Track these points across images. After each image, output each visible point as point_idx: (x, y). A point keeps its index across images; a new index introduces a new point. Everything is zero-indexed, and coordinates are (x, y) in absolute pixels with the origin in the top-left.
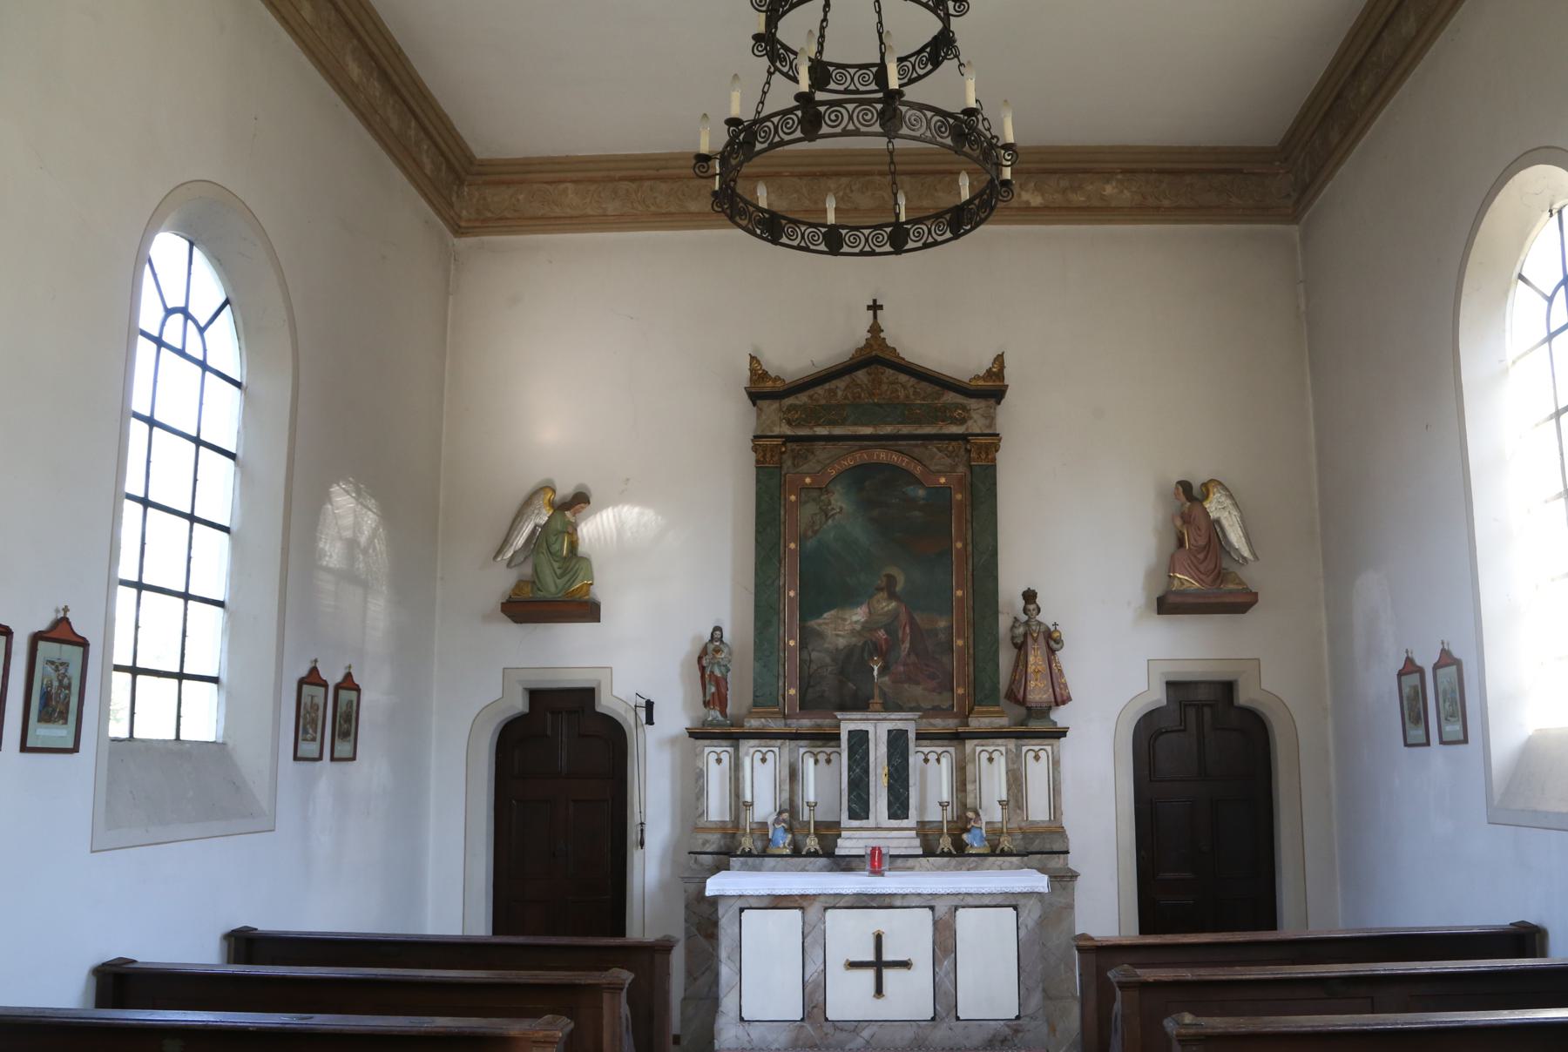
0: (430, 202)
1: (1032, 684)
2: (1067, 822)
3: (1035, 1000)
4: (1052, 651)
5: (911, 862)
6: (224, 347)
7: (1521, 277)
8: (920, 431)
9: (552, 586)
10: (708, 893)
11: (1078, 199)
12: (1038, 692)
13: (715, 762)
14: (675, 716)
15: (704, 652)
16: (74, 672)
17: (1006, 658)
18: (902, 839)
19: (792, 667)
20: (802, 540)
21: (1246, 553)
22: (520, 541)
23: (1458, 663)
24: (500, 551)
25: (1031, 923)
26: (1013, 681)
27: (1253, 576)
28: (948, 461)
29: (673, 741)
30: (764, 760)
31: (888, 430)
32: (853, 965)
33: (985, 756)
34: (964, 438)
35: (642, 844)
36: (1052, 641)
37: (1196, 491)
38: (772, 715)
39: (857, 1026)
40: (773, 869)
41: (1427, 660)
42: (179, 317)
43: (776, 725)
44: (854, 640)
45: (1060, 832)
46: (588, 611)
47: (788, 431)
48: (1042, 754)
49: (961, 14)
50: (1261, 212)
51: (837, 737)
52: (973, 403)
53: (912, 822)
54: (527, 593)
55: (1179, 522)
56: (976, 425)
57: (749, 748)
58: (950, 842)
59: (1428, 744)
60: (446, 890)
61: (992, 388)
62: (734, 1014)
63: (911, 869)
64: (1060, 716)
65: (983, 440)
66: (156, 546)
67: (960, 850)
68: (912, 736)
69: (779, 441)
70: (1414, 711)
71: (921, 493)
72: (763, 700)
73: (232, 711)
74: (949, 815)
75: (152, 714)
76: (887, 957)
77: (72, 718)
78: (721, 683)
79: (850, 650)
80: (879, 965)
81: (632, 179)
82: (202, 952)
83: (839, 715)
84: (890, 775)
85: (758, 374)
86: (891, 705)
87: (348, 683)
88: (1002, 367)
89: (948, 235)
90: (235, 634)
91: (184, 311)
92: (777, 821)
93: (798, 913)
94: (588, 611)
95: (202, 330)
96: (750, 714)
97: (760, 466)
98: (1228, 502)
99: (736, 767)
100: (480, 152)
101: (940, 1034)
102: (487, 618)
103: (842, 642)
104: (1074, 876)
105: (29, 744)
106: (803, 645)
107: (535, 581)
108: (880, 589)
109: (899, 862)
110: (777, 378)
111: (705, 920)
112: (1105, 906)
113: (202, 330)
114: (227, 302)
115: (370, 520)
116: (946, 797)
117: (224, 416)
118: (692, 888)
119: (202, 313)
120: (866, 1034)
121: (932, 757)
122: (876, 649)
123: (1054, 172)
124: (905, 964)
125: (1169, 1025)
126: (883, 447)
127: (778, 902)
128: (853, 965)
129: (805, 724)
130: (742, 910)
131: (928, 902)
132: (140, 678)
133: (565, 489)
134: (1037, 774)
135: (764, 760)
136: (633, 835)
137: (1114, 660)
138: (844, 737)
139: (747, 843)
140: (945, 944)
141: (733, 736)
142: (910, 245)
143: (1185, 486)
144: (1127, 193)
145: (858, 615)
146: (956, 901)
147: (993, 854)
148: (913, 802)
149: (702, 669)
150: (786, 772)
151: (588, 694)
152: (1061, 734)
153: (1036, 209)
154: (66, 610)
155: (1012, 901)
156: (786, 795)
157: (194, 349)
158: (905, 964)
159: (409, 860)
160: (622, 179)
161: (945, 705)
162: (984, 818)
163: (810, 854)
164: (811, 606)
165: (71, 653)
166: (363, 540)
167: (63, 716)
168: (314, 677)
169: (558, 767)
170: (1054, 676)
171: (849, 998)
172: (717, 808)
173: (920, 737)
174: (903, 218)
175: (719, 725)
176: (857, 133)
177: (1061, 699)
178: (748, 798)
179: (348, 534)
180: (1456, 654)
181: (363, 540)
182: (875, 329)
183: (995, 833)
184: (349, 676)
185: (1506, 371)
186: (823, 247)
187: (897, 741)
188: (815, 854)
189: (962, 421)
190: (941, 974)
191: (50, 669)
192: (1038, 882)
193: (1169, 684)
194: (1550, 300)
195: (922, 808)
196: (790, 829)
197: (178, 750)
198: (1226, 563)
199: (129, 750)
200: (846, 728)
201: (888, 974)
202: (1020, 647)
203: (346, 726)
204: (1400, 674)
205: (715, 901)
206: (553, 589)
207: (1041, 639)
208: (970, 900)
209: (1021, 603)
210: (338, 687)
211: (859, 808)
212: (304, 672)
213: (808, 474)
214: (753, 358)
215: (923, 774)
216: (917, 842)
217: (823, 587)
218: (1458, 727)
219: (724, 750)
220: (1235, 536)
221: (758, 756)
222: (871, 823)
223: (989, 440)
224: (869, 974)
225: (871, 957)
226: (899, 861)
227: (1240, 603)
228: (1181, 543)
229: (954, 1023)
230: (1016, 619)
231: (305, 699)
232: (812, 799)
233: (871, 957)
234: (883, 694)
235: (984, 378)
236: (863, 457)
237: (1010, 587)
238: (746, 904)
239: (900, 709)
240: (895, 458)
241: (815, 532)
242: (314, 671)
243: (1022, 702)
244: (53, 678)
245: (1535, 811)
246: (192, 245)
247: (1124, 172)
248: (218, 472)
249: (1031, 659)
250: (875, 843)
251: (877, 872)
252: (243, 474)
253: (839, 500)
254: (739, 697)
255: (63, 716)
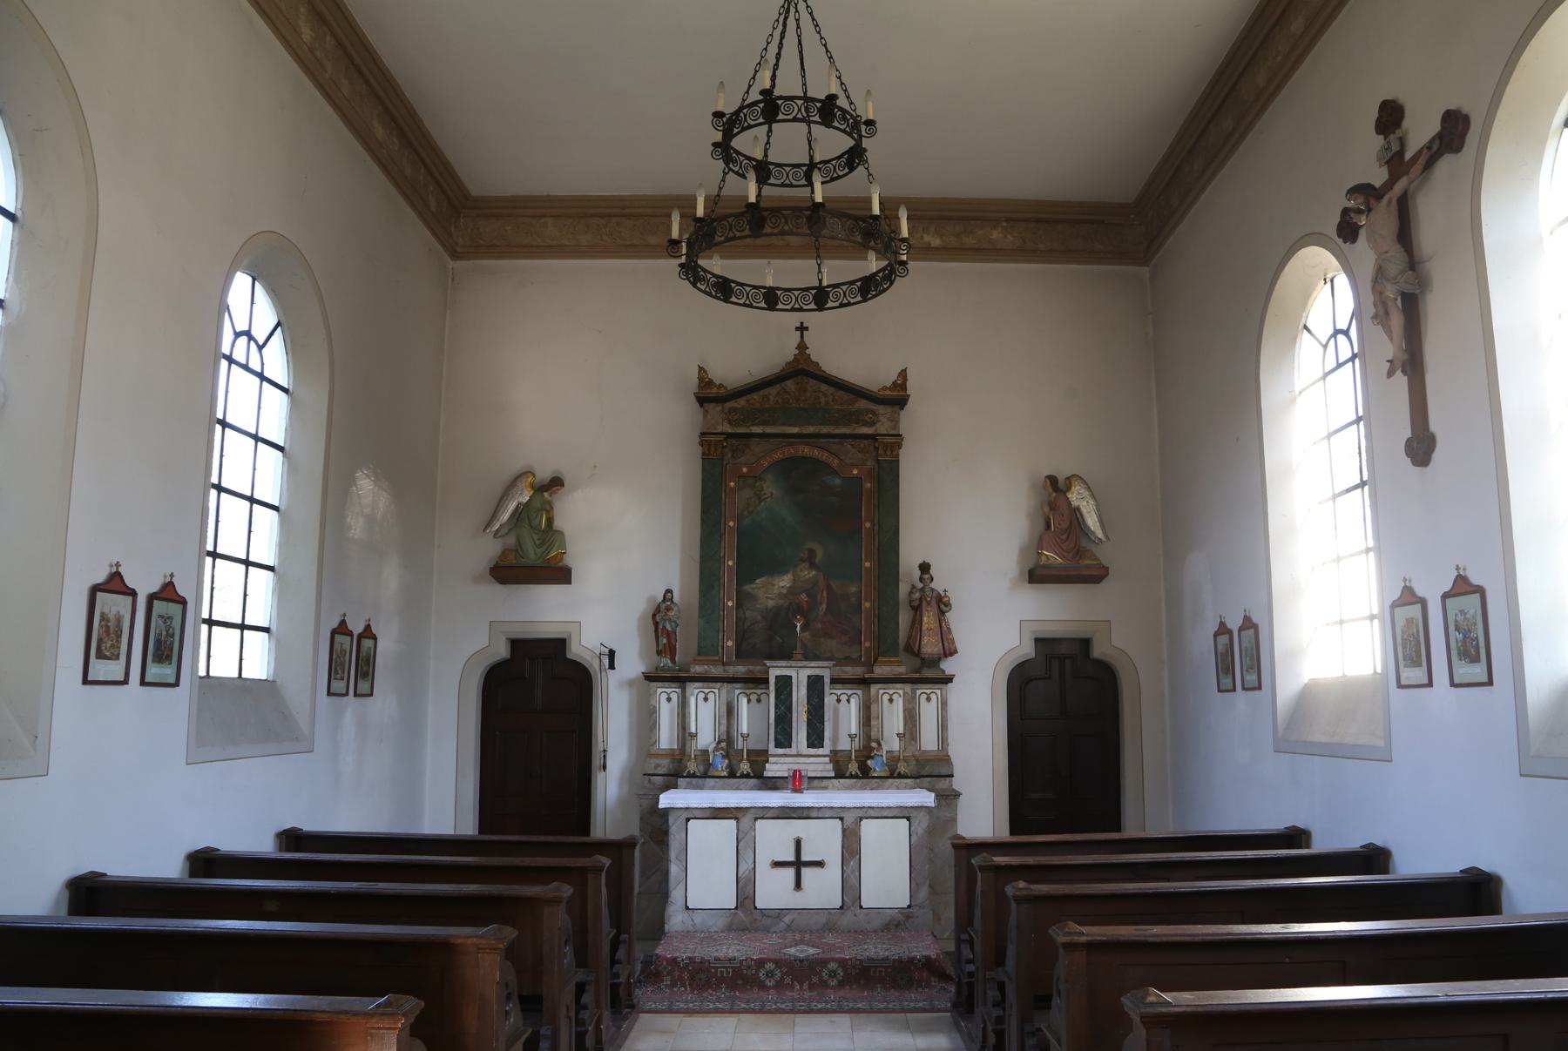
0: (435, 234)
1: (925, 639)
2: (952, 751)
3: (923, 893)
4: (943, 613)
5: (825, 783)
6: (276, 361)
7: (1305, 327)
8: (837, 431)
9: (532, 554)
10: (661, 806)
11: (970, 241)
12: (930, 645)
13: (665, 701)
14: (632, 664)
15: (658, 610)
16: (177, 624)
17: (904, 618)
18: (818, 764)
19: (729, 624)
20: (739, 519)
21: (1100, 534)
22: (505, 516)
23: (1255, 627)
24: (488, 525)
25: (920, 831)
26: (910, 637)
27: (1105, 554)
28: (860, 456)
29: (631, 683)
30: (706, 699)
31: (811, 430)
32: (777, 864)
33: (886, 697)
34: (873, 437)
35: (605, 768)
36: (942, 604)
37: (1061, 484)
38: (714, 663)
39: (780, 913)
40: (713, 788)
41: (1234, 624)
42: (244, 339)
43: (716, 671)
44: (781, 602)
45: (946, 760)
46: (561, 575)
47: (730, 430)
48: (933, 696)
49: (871, 135)
50: (1119, 255)
51: (766, 681)
52: (881, 409)
53: (826, 750)
54: (512, 560)
55: (1046, 509)
56: (882, 428)
57: (695, 692)
58: (858, 766)
59: (1234, 690)
60: (444, 804)
61: (896, 397)
62: (681, 903)
63: (825, 788)
64: (948, 666)
65: (888, 440)
66: (231, 526)
67: (865, 773)
68: (827, 680)
69: (721, 438)
70: (1225, 665)
71: (838, 481)
72: (706, 650)
73: (280, 654)
74: (856, 744)
75: (223, 656)
76: (805, 858)
77: (175, 659)
78: (671, 636)
79: (777, 611)
80: (798, 864)
81: (602, 216)
82: (262, 844)
83: (768, 663)
84: (809, 712)
85: (705, 381)
86: (810, 656)
87: (368, 633)
88: (905, 379)
89: (859, 298)
90: (283, 592)
91: (248, 334)
92: (716, 749)
93: (733, 822)
94: (561, 575)
95: (260, 348)
96: (696, 662)
97: (706, 457)
98: (1086, 493)
99: (683, 704)
100: (474, 190)
101: (847, 919)
102: (477, 579)
103: (771, 603)
104: (957, 795)
105: (148, 679)
106: (739, 605)
107: (518, 550)
108: (803, 560)
109: (816, 783)
110: (721, 386)
111: (658, 828)
112: (983, 813)
113: (260, 348)
114: (279, 324)
115: (384, 499)
116: (854, 730)
117: (275, 417)
118: (646, 803)
119: (260, 334)
120: (787, 919)
121: (844, 698)
122: (799, 610)
123: (950, 218)
124: (820, 864)
125: (1009, 890)
126: (807, 444)
127: (717, 814)
128: (777, 864)
129: (740, 670)
130: (688, 820)
131: (838, 814)
132: (214, 628)
133: (544, 473)
134: (928, 713)
135: (706, 699)
136: (596, 761)
137: (993, 623)
138: (772, 681)
139: (692, 767)
140: (851, 847)
141: (681, 679)
142: (830, 304)
143: (1052, 480)
144: (1010, 238)
145: (785, 582)
146: (861, 814)
147: (891, 777)
148: (827, 734)
149: (656, 624)
150: (724, 709)
151: (560, 644)
152: (948, 680)
153: (936, 249)
154: (172, 575)
155: (906, 813)
156: (724, 728)
157: (255, 364)
158: (820, 864)
159: (414, 776)
160: (593, 216)
161: (855, 656)
162: (885, 748)
163: (743, 776)
164: (746, 574)
165: (174, 609)
166: (379, 516)
167: (169, 658)
168: (342, 629)
169: (534, 707)
170: (944, 634)
171: (774, 890)
172: (666, 738)
173: (834, 681)
174: (825, 283)
175: (669, 670)
176: (791, 186)
177: (949, 652)
178: (693, 730)
179: (367, 511)
180: (1255, 620)
181: (379, 516)
182: (802, 347)
183: (893, 760)
184: (368, 627)
185: (1294, 400)
186: (763, 305)
187: (815, 684)
188: (747, 776)
189: (872, 424)
190: (848, 871)
191: (160, 621)
192: (927, 798)
193: (1037, 640)
194: (1325, 346)
195: (835, 739)
196: (727, 756)
197: (240, 686)
198: (1084, 543)
199: (209, 683)
200: (774, 673)
201: (805, 871)
202: (917, 609)
203: (366, 668)
204: (1216, 635)
205: (667, 811)
206: (533, 556)
207: (934, 603)
208: (872, 813)
209: (918, 573)
210: (360, 636)
211: (784, 739)
212: (335, 624)
213: (745, 465)
214: (701, 369)
215: (836, 712)
216: (830, 766)
217: (754, 563)
218: (1254, 677)
219: (674, 692)
220: (1092, 521)
221: (702, 696)
222: (793, 751)
223: (893, 440)
224: (791, 872)
225: (791, 858)
226: (815, 782)
227: (1095, 576)
228: (1048, 526)
229: (858, 911)
230: (913, 587)
231: (337, 646)
232: (745, 731)
233: (791, 858)
234: (804, 646)
235: (890, 389)
236: (790, 451)
237: (910, 557)
238: (691, 814)
239: (817, 658)
240: (816, 453)
241: (750, 513)
242: (343, 623)
243: (918, 654)
244: (147, 628)
245: (1305, 742)
246: (254, 280)
247: (1007, 220)
248: (271, 461)
249: (925, 619)
250: (796, 767)
251: (797, 790)
252: (290, 464)
253: (770, 487)
254: (685, 646)
255: (169, 658)
